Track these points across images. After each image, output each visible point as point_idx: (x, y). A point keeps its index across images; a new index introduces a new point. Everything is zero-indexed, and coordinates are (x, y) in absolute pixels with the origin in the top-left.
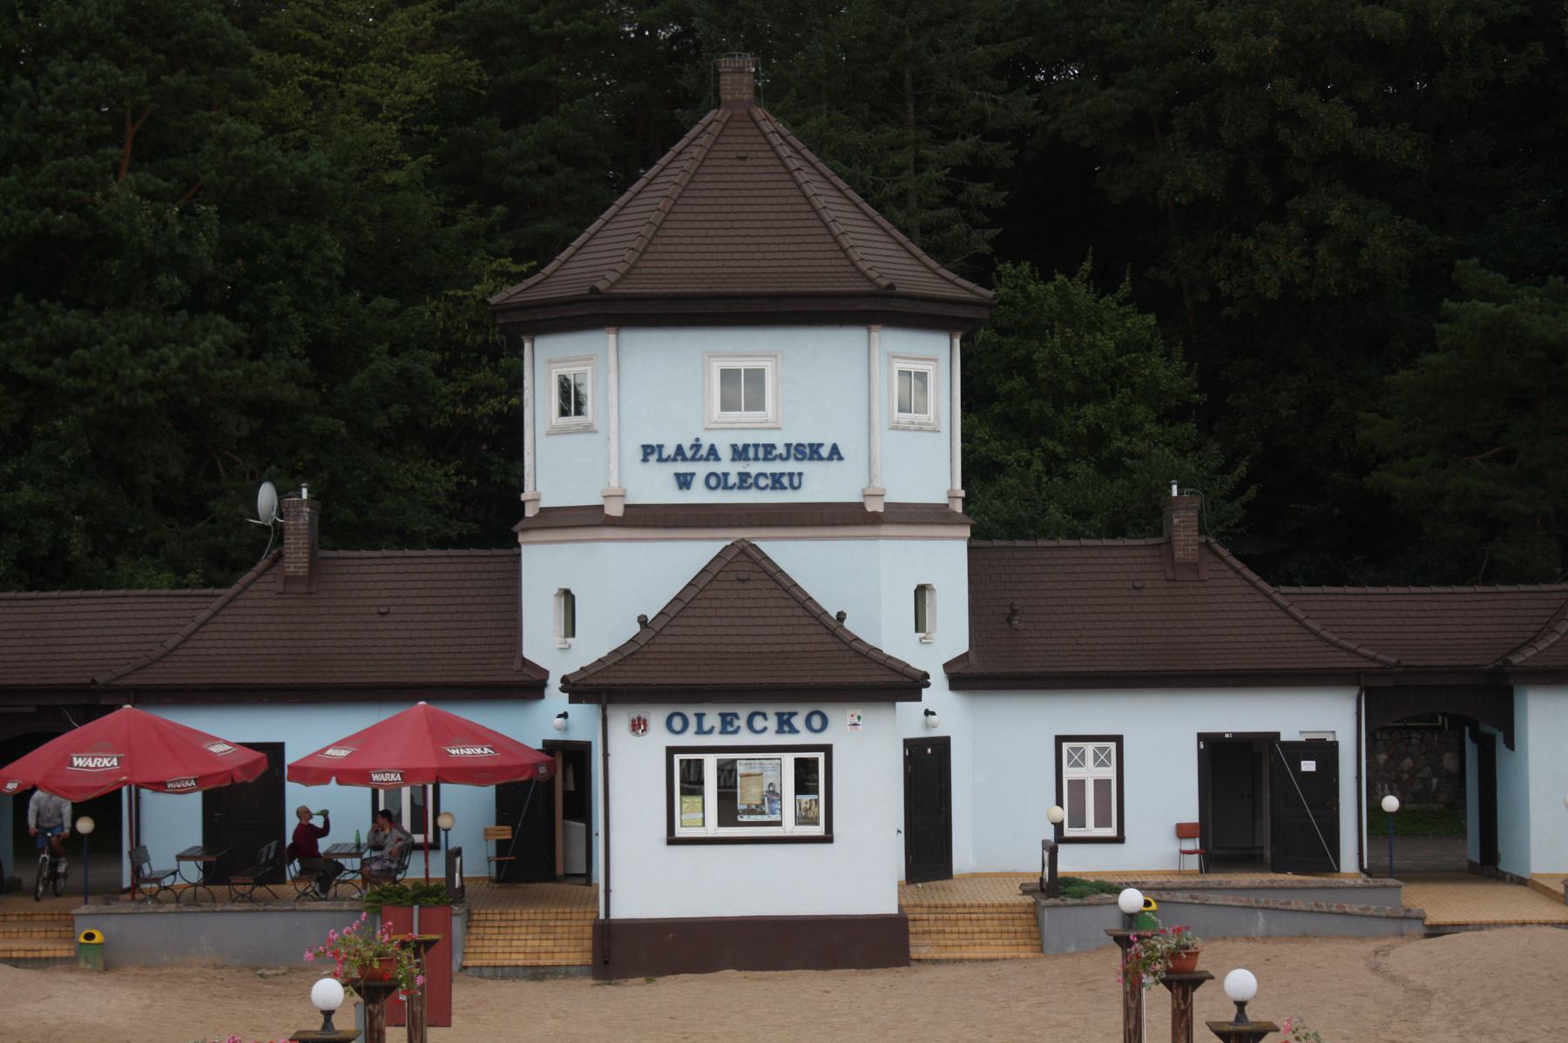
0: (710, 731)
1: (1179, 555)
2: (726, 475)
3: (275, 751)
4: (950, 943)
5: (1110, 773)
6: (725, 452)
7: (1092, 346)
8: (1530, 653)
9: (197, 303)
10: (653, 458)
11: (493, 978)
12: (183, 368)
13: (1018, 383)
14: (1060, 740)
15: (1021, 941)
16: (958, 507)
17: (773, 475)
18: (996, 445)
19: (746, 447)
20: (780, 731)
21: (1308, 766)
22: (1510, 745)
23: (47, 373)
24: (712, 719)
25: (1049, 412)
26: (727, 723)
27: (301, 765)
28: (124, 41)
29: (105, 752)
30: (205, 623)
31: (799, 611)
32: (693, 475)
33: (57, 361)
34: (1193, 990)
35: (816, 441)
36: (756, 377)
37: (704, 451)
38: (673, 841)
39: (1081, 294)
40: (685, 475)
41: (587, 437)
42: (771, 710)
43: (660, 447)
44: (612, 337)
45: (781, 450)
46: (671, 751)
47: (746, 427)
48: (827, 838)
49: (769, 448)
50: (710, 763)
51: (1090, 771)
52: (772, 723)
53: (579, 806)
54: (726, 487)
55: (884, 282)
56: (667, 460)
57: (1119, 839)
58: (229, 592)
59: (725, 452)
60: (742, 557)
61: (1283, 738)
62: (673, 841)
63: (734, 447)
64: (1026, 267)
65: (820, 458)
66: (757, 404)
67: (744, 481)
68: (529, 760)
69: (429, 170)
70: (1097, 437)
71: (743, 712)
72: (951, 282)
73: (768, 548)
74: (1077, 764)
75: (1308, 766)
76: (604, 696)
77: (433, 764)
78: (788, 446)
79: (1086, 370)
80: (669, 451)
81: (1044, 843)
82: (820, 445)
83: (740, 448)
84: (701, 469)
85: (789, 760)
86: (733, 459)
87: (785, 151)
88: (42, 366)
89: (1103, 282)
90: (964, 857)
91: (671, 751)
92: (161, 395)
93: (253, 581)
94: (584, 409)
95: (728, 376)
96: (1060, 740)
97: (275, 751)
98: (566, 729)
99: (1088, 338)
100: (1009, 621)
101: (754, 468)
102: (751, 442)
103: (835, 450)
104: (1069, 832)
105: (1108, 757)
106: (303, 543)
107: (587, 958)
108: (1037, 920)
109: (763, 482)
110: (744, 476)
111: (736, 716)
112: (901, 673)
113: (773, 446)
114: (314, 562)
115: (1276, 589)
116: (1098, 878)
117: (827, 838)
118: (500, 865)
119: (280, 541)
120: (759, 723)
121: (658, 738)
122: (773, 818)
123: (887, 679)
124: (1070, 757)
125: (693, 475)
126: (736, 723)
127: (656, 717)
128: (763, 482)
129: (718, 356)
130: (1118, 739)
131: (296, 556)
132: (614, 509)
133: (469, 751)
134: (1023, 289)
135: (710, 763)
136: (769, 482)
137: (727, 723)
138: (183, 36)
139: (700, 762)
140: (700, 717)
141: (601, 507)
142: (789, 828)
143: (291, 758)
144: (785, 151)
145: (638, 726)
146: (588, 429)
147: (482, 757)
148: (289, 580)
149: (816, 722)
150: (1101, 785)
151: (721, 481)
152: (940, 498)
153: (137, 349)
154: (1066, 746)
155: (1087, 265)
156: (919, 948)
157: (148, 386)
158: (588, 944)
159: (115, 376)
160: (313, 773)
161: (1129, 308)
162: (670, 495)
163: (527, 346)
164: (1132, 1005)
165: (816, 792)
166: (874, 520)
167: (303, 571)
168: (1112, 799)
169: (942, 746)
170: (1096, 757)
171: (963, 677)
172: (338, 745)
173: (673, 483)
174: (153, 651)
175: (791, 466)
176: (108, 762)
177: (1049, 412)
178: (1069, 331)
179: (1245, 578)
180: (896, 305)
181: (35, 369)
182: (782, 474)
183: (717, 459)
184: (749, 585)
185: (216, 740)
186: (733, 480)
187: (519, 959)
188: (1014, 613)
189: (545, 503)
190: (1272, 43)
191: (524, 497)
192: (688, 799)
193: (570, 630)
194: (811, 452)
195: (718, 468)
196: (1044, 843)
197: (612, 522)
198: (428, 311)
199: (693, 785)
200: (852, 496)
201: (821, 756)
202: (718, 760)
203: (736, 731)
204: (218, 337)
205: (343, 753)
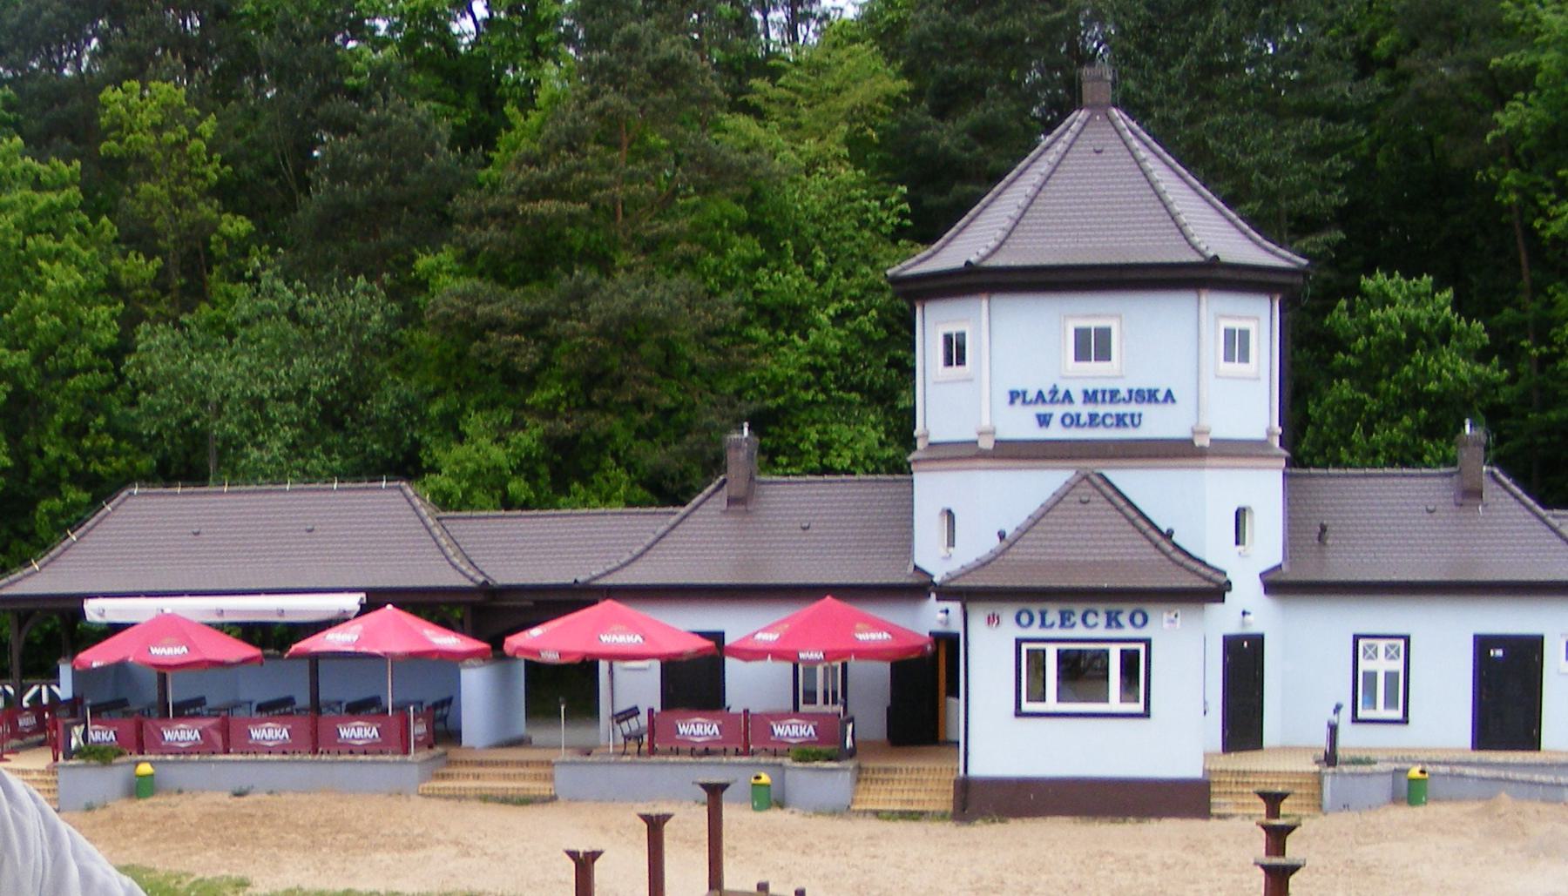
0: (1052, 625)
3: (718, 637)
4: (1246, 801)
5: (1398, 665)
6: (1077, 396)
10: (1018, 401)
15: (1305, 802)
17: (1118, 415)
19: (1095, 393)
20: (1109, 625)
24: (1053, 616)
27: (737, 646)
30: (664, 535)
32: (1051, 415)
35: (1153, 387)
36: (1104, 335)
37: (1060, 395)
40: (1045, 416)
42: (1102, 608)
44: (984, 303)
47: (1095, 374)
48: (1146, 714)
49: (1114, 394)
51: (1381, 664)
52: (1102, 619)
54: (1078, 424)
55: (1211, 253)
56: (1031, 402)
57: (1405, 720)
58: (682, 511)
59: (1077, 396)
60: (1085, 483)
63: (1086, 393)
68: (921, 643)
71: (1079, 609)
72: (1273, 253)
73: (1116, 476)
78: (1130, 392)
80: (1031, 395)
82: (1156, 391)
83: (1090, 392)
84: (1058, 411)
86: (1085, 402)
87: (1136, 144)
91: (1019, 643)
94: (964, 358)
95: (1081, 336)
96: (1356, 638)
97: (718, 637)
98: (947, 623)
101: (1101, 410)
103: (1169, 395)
105: (1398, 652)
107: (951, 809)
110: (1093, 417)
111: (1073, 613)
113: (1118, 391)
115: (1550, 512)
116: (1352, 753)
123: (1195, 585)
125: (1051, 415)
126: (1073, 619)
127: (1008, 613)
128: (1108, 421)
129: (1072, 317)
136: (1115, 421)
137: (1065, 620)
141: (976, 442)
143: (728, 641)
144: (1136, 144)
145: (993, 620)
147: (882, 641)
149: (1139, 619)
150: (1391, 677)
151: (1075, 421)
152: (1259, 434)
160: (750, 654)
162: (1034, 432)
163: (919, 310)
168: (1400, 688)
169: (1257, 642)
170: (1387, 652)
172: (765, 630)
173: (1035, 422)
175: (1133, 408)
180: (1222, 274)
182: (1124, 415)
184: (1087, 506)
186: (1084, 419)
189: (933, 438)
191: (916, 433)
193: (951, 542)
194: (1150, 396)
195: (1072, 409)
197: (983, 455)
201: (1142, 647)
202: (1482, 644)
203: (1073, 625)
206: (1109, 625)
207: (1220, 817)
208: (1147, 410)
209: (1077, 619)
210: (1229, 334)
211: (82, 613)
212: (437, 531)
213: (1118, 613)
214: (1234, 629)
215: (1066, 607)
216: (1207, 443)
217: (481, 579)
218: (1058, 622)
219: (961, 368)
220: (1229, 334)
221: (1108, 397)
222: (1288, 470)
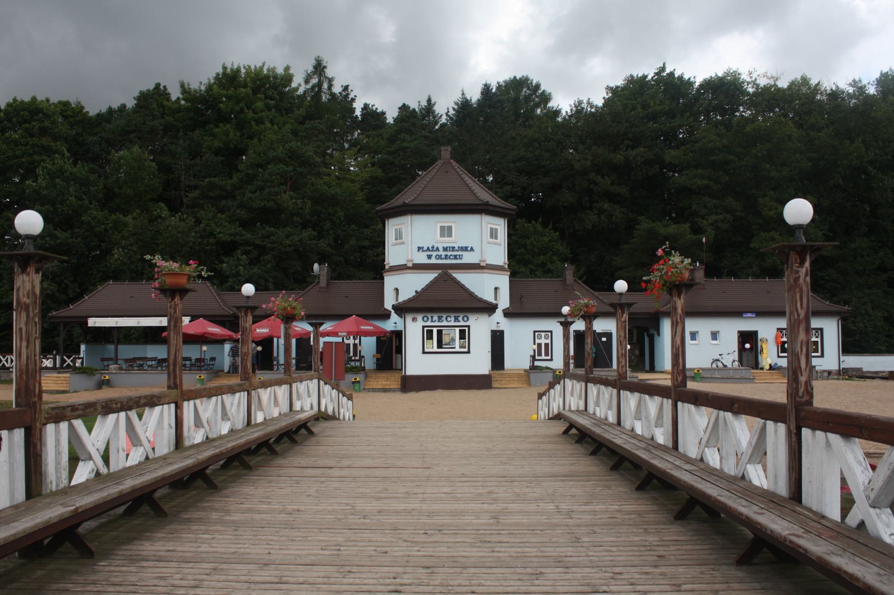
0: (435, 321)
1: (568, 282)
2: (441, 255)
5: (548, 341)
6: (441, 249)
7: (542, 241)
8: (665, 308)
9: (304, 226)
10: (421, 250)
11: (373, 392)
12: (299, 241)
13: (522, 250)
14: (535, 332)
16: (506, 266)
18: (517, 267)
19: (447, 247)
20: (455, 321)
21: (604, 339)
22: (659, 335)
23: (264, 243)
24: (436, 318)
25: (531, 258)
26: (440, 319)
28: (287, 160)
29: (266, 328)
31: (461, 289)
33: (267, 240)
34: (594, 320)
36: (450, 228)
37: (435, 249)
38: (424, 352)
39: (539, 228)
41: (403, 245)
42: (452, 315)
43: (423, 247)
44: (410, 217)
45: (457, 248)
46: (424, 327)
47: (447, 242)
48: (468, 352)
49: (453, 248)
50: (435, 330)
52: (453, 319)
53: (399, 350)
54: (441, 259)
55: (485, 201)
56: (425, 251)
59: (441, 249)
61: (597, 332)
62: (424, 352)
63: (443, 247)
64: (524, 220)
65: (468, 251)
66: (450, 235)
67: (446, 257)
69: (367, 194)
70: (543, 265)
74: (539, 339)
75: (604, 339)
76: (404, 311)
77: (356, 330)
78: (459, 247)
79: (540, 247)
80: (425, 248)
81: (531, 356)
84: (434, 254)
85: (457, 330)
88: (263, 241)
89: (545, 225)
90: (508, 363)
91: (424, 327)
92: (293, 248)
93: (311, 288)
95: (442, 228)
96: (535, 332)
98: (396, 327)
99: (541, 239)
100: (521, 299)
101: (449, 253)
102: (448, 246)
104: (537, 358)
106: (325, 278)
107: (400, 386)
108: (528, 377)
109: (451, 257)
110: (446, 256)
111: (442, 317)
112: (490, 305)
113: (454, 247)
114: (328, 284)
117: (468, 352)
118: (377, 364)
119: (319, 278)
120: (449, 319)
121: (420, 323)
122: (453, 346)
124: (538, 337)
127: (419, 317)
128: (451, 257)
130: (551, 332)
131: (323, 282)
132: (410, 265)
133: (367, 328)
134: (524, 226)
135: (435, 330)
137: (440, 319)
138: (303, 159)
139: (432, 330)
140: (432, 317)
142: (457, 349)
145: (414, 320)
146: (403, 243)
148: (321, 288)
149: (465, 319)
151: (440, 257)
152: (502, 264)
153: (287, 237)
154: (536, 334)
155: (540, 219)
156: (495, 385)
157: (290, 246)
158: (400, 383)
159: (281, 244)
161: (552, 231)
164: (567, 347)
165: (465, 339)
166: (483, 268)
167: (325, 285)
169: (502, 332)
170: (545, 337)
171: (507, 314)
173: (426, 257)
174: (321, 360)
176: (266, 330)
177: (531, 258)
178: (536, 236)
179: (586, 289)
181: (261, 242)
183: (439, 251)
185: (297, 327)
186: (443, 256)
187: (380, 387)
188: (522, 297)
189: (391, 265)
190: (589, 163)
191: (385, 263)
192: (428, 341)
194: (465, 249)
196: (531, 356)
197: (409, 268)
198: (367, 231)
199: (430, 337)
200: (477, 261)
201: (467, 329)
203: (442, 321)
204: (309, 233)
205: (331, 328)
206: (455, 321)
207: (495, 388)
208: (464, 253)
209: (444, 319)
210: (491, 229)
211: (87, 323)
212: (217, 297)
213: (459, 316)
214: (495, 328)
215: (440, 315)
216: (485, 265)
217: (232, 312)
218: (437, 320)
219: (450, 239)
220: (491, 229)
221: (451, 249)
222: (511, 279)
